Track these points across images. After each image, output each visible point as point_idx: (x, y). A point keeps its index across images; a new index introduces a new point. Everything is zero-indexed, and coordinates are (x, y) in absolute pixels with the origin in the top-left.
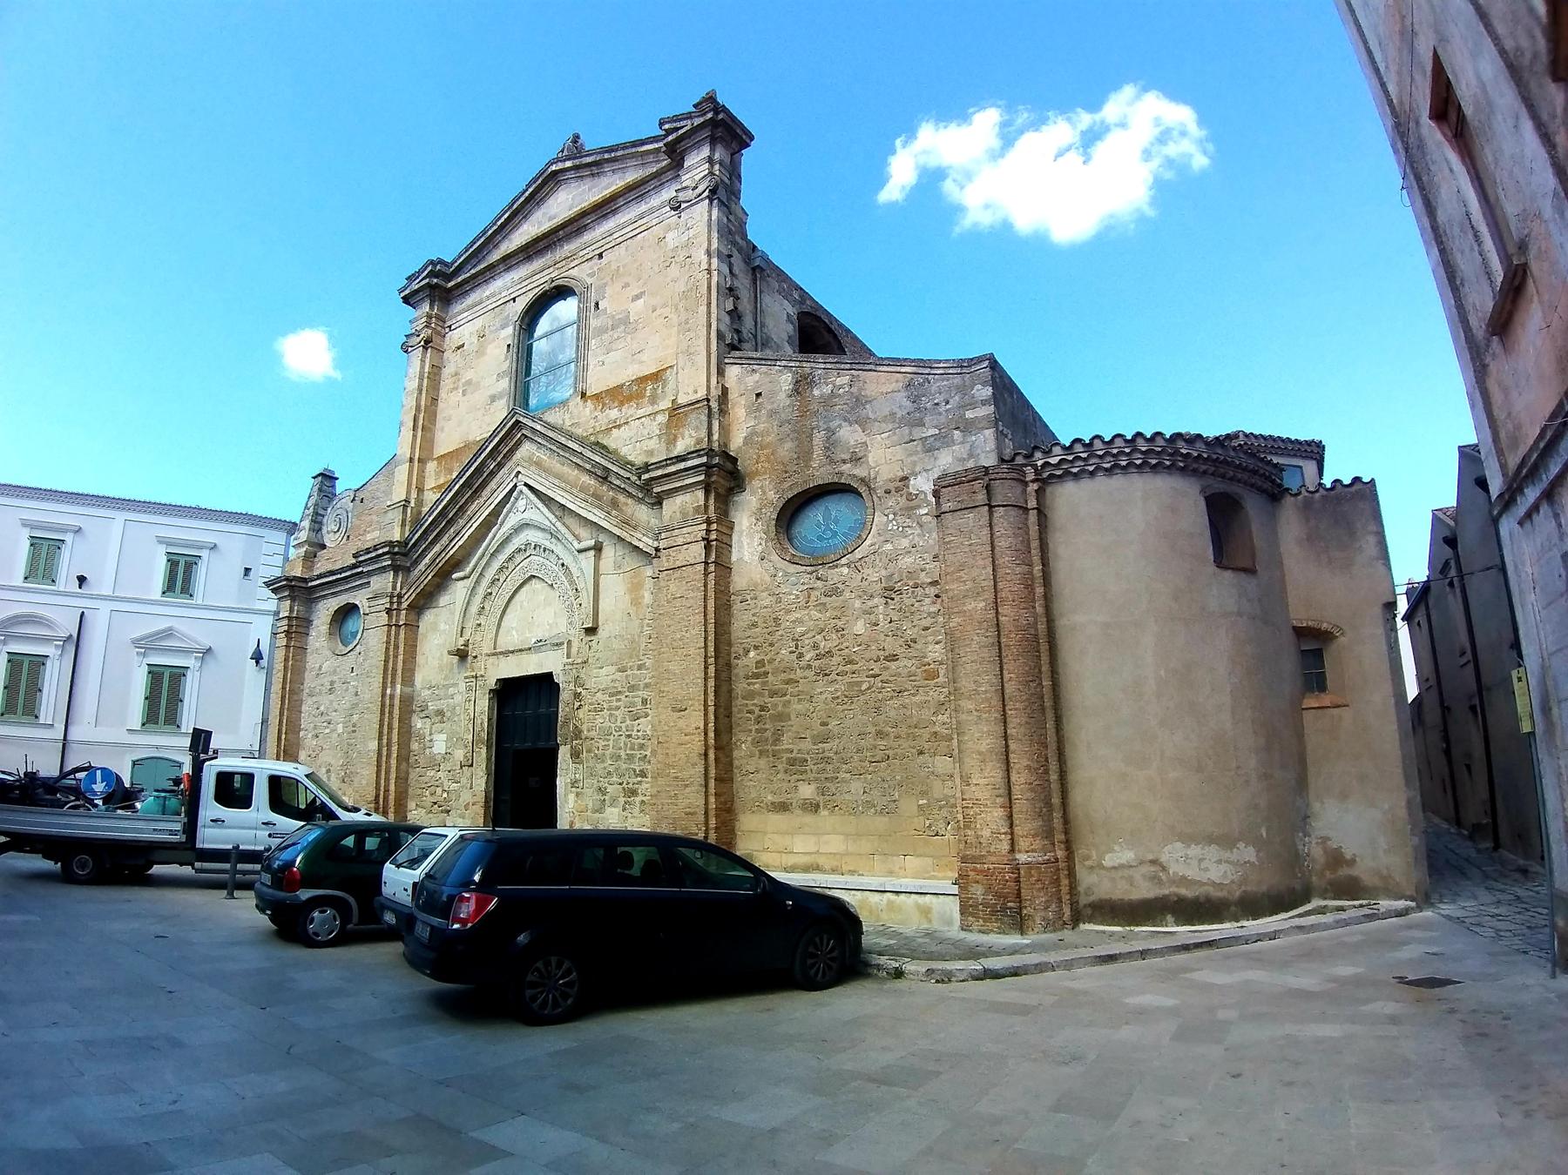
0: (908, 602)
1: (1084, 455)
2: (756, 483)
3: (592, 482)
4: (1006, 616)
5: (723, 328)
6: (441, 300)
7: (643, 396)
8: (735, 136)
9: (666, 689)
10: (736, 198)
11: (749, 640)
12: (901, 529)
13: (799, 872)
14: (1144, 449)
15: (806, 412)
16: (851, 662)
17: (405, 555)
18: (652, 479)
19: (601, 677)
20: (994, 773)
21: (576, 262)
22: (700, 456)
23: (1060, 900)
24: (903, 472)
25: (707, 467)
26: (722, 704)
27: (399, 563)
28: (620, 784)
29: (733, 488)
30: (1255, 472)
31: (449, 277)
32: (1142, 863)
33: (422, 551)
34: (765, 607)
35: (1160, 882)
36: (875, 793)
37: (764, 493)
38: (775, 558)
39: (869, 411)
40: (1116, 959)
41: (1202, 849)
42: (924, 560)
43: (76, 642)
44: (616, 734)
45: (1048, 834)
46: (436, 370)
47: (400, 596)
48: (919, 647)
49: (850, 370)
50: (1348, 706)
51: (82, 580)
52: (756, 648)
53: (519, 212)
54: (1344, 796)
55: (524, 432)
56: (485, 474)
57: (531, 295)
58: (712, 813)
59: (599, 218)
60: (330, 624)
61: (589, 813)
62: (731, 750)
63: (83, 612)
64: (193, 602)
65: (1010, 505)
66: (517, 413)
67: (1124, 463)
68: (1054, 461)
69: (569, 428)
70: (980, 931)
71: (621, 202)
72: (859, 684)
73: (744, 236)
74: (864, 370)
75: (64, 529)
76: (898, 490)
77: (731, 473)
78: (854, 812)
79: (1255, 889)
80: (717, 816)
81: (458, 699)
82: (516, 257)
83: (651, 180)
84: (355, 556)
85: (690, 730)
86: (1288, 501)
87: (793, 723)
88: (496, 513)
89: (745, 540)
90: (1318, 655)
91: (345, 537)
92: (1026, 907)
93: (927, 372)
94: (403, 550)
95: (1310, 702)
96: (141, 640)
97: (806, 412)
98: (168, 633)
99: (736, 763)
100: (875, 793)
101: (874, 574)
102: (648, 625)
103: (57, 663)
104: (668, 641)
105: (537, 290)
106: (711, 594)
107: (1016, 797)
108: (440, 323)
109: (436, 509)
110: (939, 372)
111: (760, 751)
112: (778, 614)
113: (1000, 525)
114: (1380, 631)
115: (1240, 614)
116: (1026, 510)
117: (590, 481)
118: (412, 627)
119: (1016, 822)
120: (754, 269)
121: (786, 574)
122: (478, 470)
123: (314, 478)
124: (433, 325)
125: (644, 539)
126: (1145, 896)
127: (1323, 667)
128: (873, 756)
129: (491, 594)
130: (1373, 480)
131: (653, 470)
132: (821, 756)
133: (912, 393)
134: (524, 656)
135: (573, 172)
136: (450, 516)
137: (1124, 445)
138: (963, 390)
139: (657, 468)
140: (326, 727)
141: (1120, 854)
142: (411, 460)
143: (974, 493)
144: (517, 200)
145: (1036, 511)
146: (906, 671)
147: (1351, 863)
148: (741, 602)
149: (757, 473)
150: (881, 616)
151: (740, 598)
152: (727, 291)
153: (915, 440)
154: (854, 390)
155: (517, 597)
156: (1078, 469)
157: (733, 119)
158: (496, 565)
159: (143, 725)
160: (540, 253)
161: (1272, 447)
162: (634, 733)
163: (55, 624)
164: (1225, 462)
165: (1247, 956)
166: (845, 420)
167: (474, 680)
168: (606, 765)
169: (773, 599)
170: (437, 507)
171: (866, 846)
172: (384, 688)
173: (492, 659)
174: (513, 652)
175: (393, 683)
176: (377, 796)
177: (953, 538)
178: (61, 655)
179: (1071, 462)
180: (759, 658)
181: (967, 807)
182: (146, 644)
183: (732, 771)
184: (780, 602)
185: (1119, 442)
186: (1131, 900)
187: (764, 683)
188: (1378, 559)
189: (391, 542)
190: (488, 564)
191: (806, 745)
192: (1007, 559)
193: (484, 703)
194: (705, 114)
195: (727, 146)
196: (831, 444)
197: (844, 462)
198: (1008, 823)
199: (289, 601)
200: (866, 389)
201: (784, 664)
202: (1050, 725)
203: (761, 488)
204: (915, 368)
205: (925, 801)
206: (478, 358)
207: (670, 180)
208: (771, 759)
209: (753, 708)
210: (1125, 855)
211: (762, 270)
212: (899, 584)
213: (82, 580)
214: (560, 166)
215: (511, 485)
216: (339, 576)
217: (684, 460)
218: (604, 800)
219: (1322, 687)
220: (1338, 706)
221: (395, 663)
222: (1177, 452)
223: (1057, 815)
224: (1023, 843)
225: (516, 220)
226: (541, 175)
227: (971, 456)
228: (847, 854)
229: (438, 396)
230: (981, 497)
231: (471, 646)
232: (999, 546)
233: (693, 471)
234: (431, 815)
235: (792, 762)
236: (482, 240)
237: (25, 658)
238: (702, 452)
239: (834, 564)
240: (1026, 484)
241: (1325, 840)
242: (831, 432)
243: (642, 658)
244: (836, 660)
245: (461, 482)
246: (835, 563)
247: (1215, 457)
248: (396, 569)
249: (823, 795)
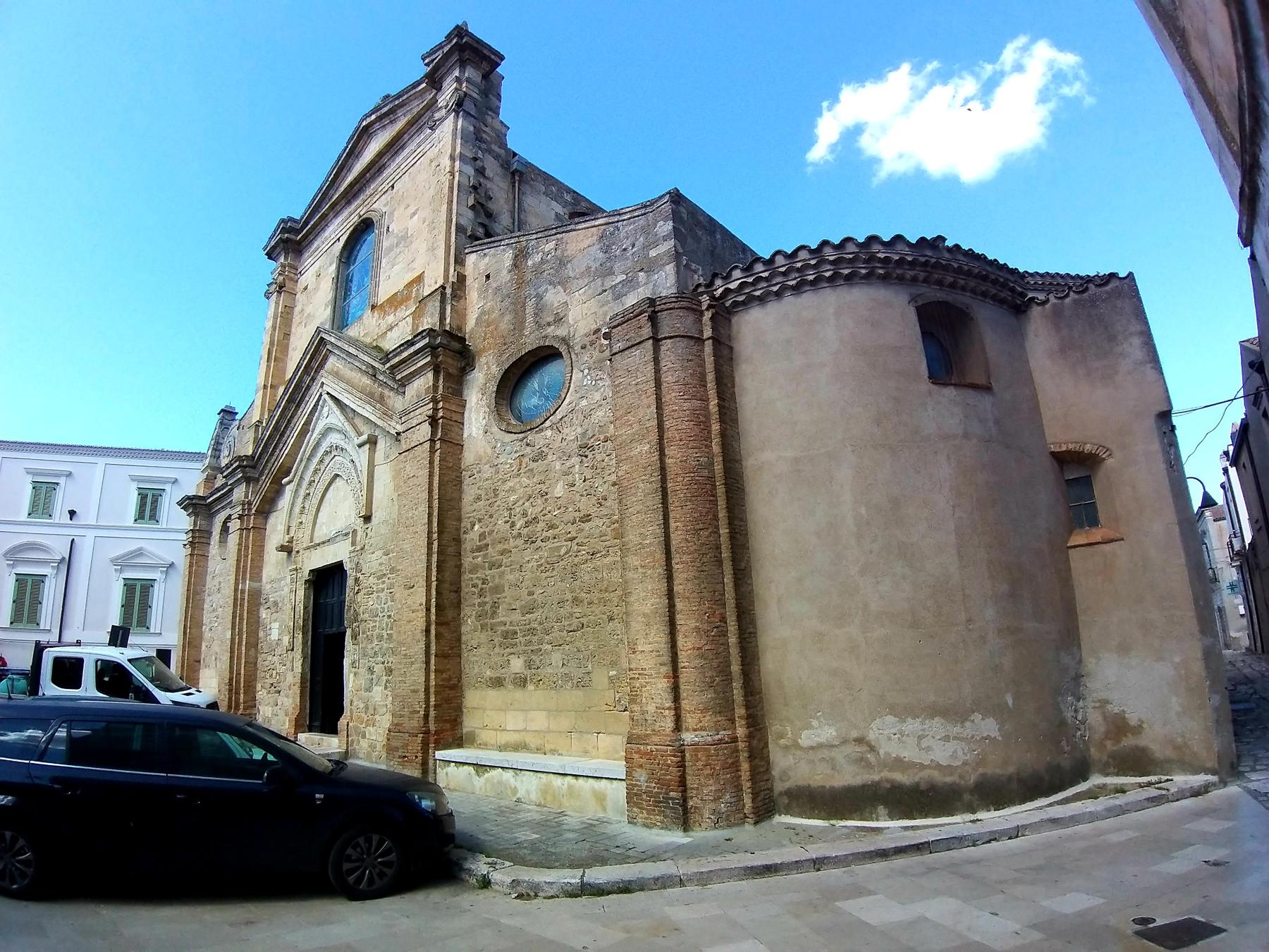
0: (599, 457)
1: (765, 275)
2: (483, 360)
3: (368, 382)
4: (672, 458)
5: (463, 222)
6: (294, 251)
8: (485, 58)
9: (401, 567)
10: (494, 113)
12: (594, 383)
13: (510, 751)
14: (831, 258)
15: (522, 283)
16: (552, 527)
17: (254, 467)
19: (373, 561)
20: (656, 638)
21: (378, 197)
22: (424, 338)
23: (739, 788)
25: (431, 347)
26: (448, 579)
27: (248, 475)
29: (464, 367)
30: (985, 278)
31: (298, 232)
32: (844, 742)
35: (869, 766)
36: (573, 664)
37: (489, 368)
38: (495, 429)
39: (570, 271)
40: (776, 871)
41: (922, 723)
43: (68, 563)
45: (724, 707)
47: (250, 503)
48: (608, 504)
49: (556, 234)
50: (1123, 539)
51: (72, 513)
52: (480, 521)
53: (344, 167)
54: (1124, 649)
55: (328, 347)
58: (432, 690)
59: (393, 156)
62: (459, 626)
63: (73, 539)
64: (159, 526)
65: (677, 336)
66: (321, 331)
67: (811, 278)
68: (733, 286)
69: (362, 338)
70: (645, 825)
73: (503, 145)
75: (58, 474)
76: (592, 344)
77: (460, 353)
78: (555, 686)
79: (998, 771)
80: (436, 693)
81: (286, 590)
85: (416, 607)
86: (1036, 311)
88: (308, 423)
89: (473, 416)
90: (1086, 483)
92: (692, 797)
93: (616, 220)
94: (251, 463)
95: (1078, 539)
96: (119, 559)
97: (522, 283)
98: (139, 553)
99: (464, 638)
100: (573, 664)
101: (572, 432)
103: (163, 585)
106: (437, 470)
107: (683, 665)
108: (293, 271)
110: (625, 218)
111: (481, 625)
112: (496, 484)
113: (667, 359)
114: (1156, 447)
115: (966, 436)
116: (700, 341)
117: (366, 381)
119: (683, 695)
120: (513, 174)
123: (219, 414)
124: (286, 273)
126: (850, 782)
127: (1093, 497)
128: (570, 625)
129: (309, 494)
130: (1131, 274)
132: (528, 627)
133: (604, 244)
135: (378, 124)
137: (808, 257)
138: (646, 231)
140: (216, 621)
141: (819, 731)
144: (341, 157)
145: (711, 341)
146: (598, 531)
147: (1138, 730)
148: (470, 477)
149: (484, 350)
151: (469, 473)
152: (471, 189)
153: (606, 290)
154: (559, 252)
156: (761, 291)
157: (479, 41)
158: (312, 468)
159: (11, 623)
160: (355, 196)
161: (1050, 284)
163: (52, 550)
164: (937, 265)
165: (953, 867)
166: (550, 284)
167: (295, 572)
169: (493, 470)
171: (565, 723)
172: (237, 584)
175: (244, 579)
176: (231, 679)
177: (622, 380)
178: (57, 573)
179: (753, 284)
180: (482, 530)
181: (633, 678)
182: (122, 563)
183: (460, 646)
185: (803, 255)
186: (833, 787)
187: (485, 556)
188: (1142, 363)
189: (240, 456)
190: (306, 467)
191: (516, 616)
192: (674, 394)
194: (451, 41)
195: (477, 67)
197: (549, 324)
198: (671, 697)
200: (567, 250)
202: (728, 580)
203: (487, 363)
204: (607, 219)
205: (615, 673)
208: (490, 633)
210: (827, 733)
211: (521, 174)
212: (592, 440)
213: (72, 513)
214: (369, 120)
217: (413, 344)
219: (1094, 522)
220: (1112, 541)
221: (246, 562)
222: (872, 258)
223: (737, 686)
224: (690, 720)
228: (549, 731)
229: (290, 331)
230: (647, 331)
232: (666, 382)
234: (270, 695)
235: (506, 635)
237: (136, 582)
238: (424, 334)
239: (538, 428)
240: (701, 313)
241: (1105, 702)
242: (539, 297)
244: (541, 525)
246: (540, 427)
247: (923, 259)
248: (248, 480)
249: (530, 669)
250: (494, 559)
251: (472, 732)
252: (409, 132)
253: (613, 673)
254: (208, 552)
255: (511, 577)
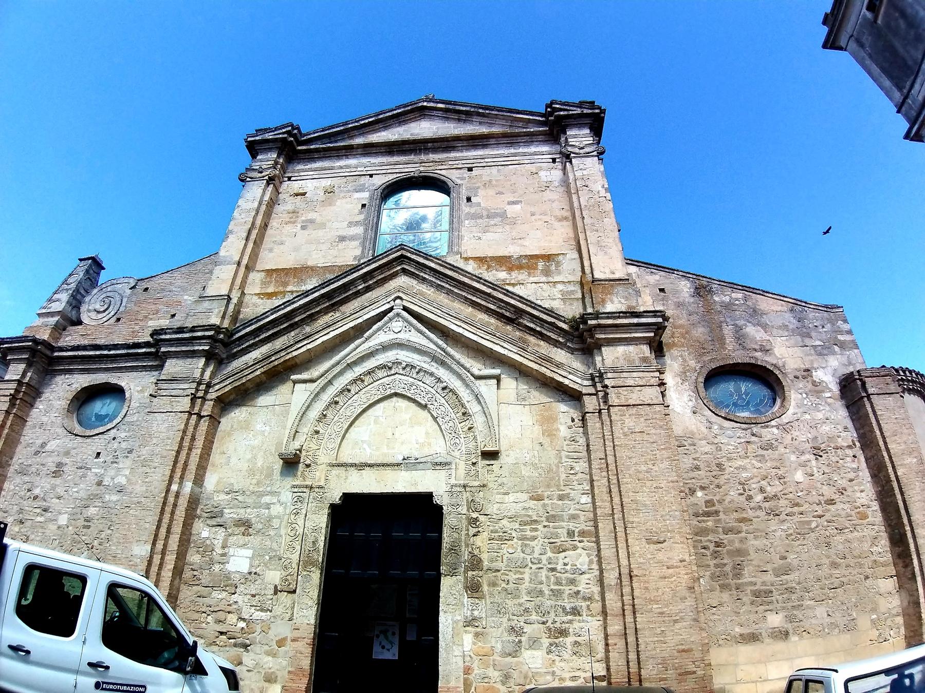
0: (834, 459)
7: (536, 269)
9: (636, 520)
11: (693, 480)
16: (797, 505)
18: (599, 326)
22: (655, 316)
24: (805, 365)
28: (543, 623)
33: (247, 347)
34: (706, 453)
42: (838, 429)
44: (534, 567)
46: (272, 203)
52: (702, 488)
56: (351, 292)
57: (391, 177)
59: (468, 146)
60: (72, 401)
61: (496, 657)
71: (493, 141)
72: (809, 522)
74: (753, 293)
82: (378, 148)
83: (525, 136)
84: (155, 333)
85: (674, 562)
87: (752, 558)
91: (114, 319)
102: (568, 457)
104: (631, 472)
105: (399, 175)
109: (283, 309)
118: (214, 421)
121: (721, 428)
122: (345, 287)
125: (571, 377)
131: (602, 318)
134: (389, 473)
135: (441, 112)
136: (297, 319)
139: (608, 318)
142: (239, 264)
143: (887, 384)
149: (674, 345)
150: (815, 469)
155: (370, 412)
158: (350, 376)
162: (559, 567)
168: (522, 601)
169: (714, 447)
170: (285, 307)
173: (336, 471)
174: (371, 466)
180: (708, 498)
184: (721, 450)
190: (341, 373)
191: (769, 577)
193: (321, 520)
196: (740, 337)
199: (25, 365)
201: (735, 505)
206: (323, 206)
207: (539, 141)
209: (708, 543)
215: (387, 306)
216: (106, 352)
218: (520, 642)
225: (377, 126)
226: (411, 105)
227: (850, 364)
231: (304, 453)
233: (644, 327)
235: (757, 594)
236: (342, 128)
243: (563, 488)
244: (783, 502)
245: (323, 291)
248: (209, 356)
249: (791, 622)
250: (731, 525)
251: (721, 688)
252: (499, 139)
253: (874, 617)
254: (27, 415)
255: (756, 543)
